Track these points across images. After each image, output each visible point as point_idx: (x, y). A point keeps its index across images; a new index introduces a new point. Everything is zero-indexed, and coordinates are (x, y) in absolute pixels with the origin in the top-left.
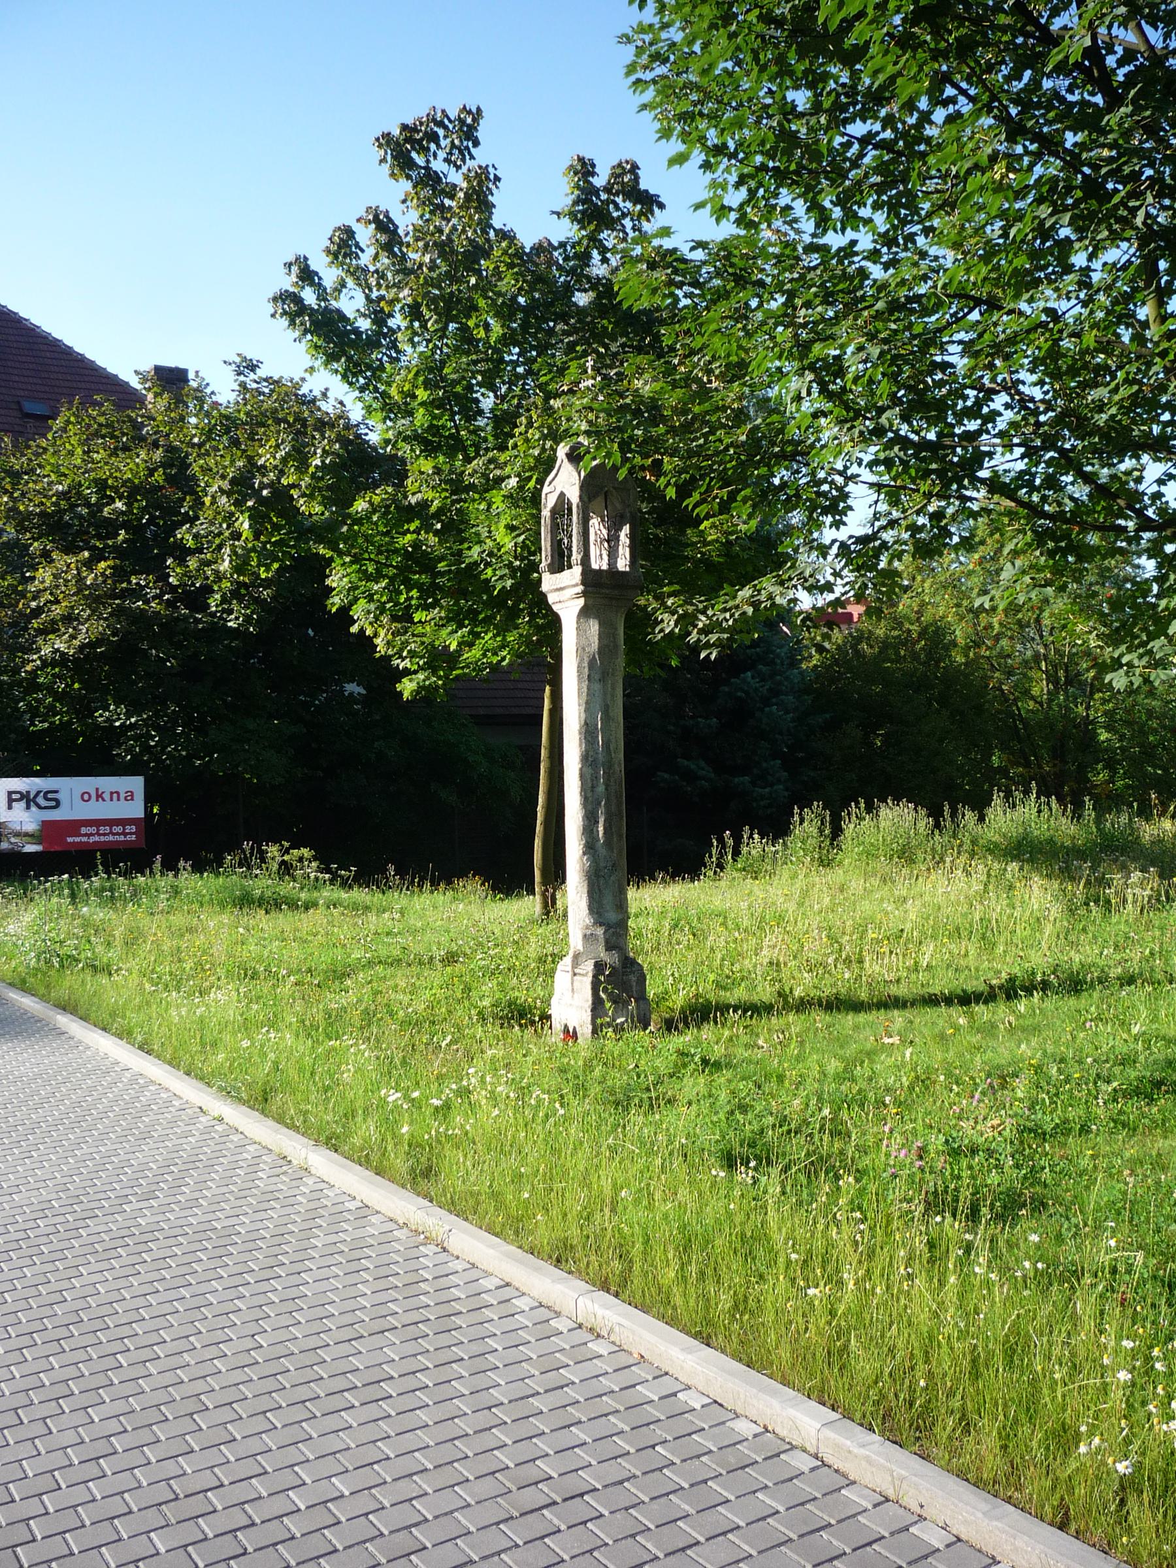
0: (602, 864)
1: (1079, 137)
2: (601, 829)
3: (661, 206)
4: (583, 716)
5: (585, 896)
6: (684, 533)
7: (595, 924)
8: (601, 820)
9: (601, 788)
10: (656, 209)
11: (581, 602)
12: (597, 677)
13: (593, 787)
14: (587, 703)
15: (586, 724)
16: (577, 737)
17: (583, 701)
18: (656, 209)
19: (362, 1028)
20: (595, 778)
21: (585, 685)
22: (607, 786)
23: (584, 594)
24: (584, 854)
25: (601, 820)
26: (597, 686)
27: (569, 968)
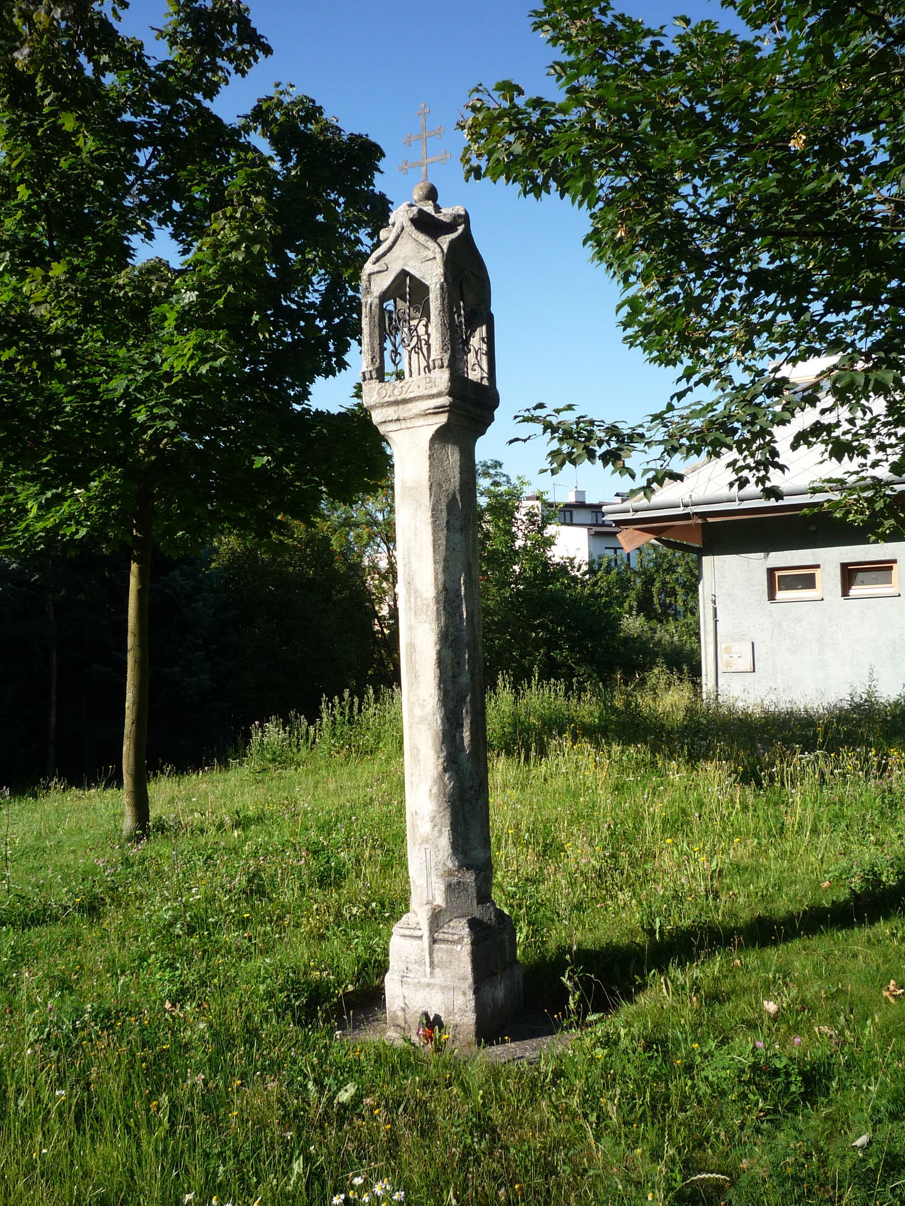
0: (468, 784)
1: (618, 235)
2: (466, 735)
3: (426, 1015)
4: (441, 577)
5: (446, 832)
6: (895, 391)
7: (460, 867)
8: (467, 722)
9: (465, 679)
10: (432, 1018)
11: (443, 419)
12: (458, 524)
13: (454, 677)
14: (446, 560)
15: (445, 588)
16: (433, 607)
17: (441, 558)
18: (432, 1018)
19: (59, 1155)
20: (457, 663)
21: (443, 534)
22: (473, 674)
23: (451, 410)
24: (445, 770)
25: (467, 722)
26: (457, 537)
27: (425, 931)
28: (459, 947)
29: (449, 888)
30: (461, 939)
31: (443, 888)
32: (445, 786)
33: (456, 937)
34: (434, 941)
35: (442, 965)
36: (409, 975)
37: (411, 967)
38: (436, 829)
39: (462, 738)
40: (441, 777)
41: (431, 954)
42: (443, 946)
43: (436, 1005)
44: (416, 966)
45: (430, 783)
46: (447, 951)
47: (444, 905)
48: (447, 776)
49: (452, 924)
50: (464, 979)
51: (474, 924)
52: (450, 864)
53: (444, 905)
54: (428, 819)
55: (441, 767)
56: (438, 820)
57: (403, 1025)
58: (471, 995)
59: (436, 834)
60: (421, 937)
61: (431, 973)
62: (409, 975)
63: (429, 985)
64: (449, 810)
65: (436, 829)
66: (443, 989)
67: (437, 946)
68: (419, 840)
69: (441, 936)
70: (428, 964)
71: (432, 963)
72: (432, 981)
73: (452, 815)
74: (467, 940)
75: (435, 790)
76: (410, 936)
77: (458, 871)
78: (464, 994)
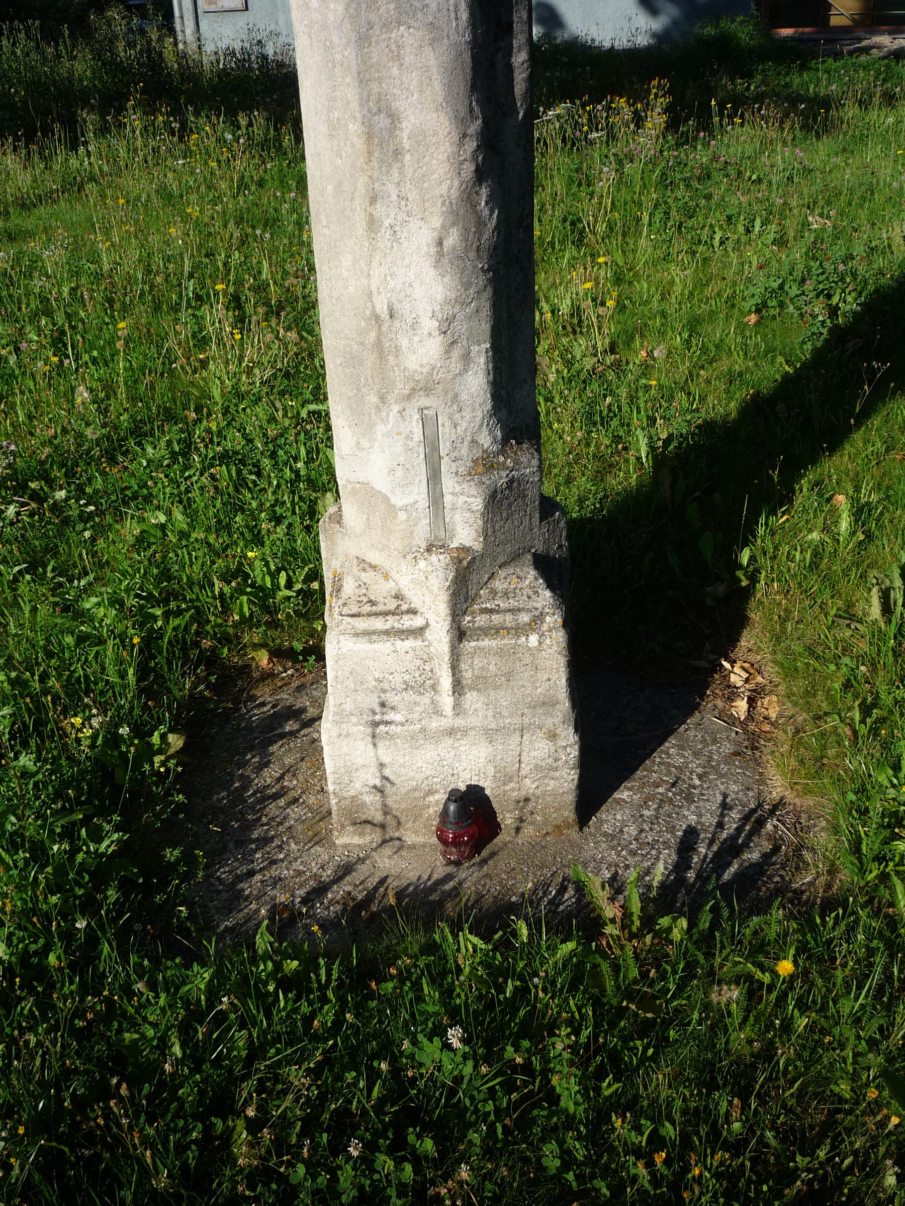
24: (480, 175)
28: (534, 639)
29: (496, 503)
30: (539, 618)
31: (478, 504)
32: (480, 223)
33: (525, 618)
34: (460, 635)
35: (482, 683)
36: (391, 716)
37: (392, 699)
38: (456, 353)
39: (510, 69)
40: (468, 197)
41: (455, 667)
42: (486, 643)
43: (471, 763)
44: (410, 696)
45: (437, 221)
46: (499, 652)
47: (478, 546)
48: (484, 192)
49: (499, 585)
50: (548, 703)
51: (544, 565)
52: (485, 440)
53: (478, 546)
54: (429, 325)
55: (469, 169)
56: (461, 327)
57: (378, 817)
58: (569, 738)
59: (455, 365)
60: (419, 632)
61: (457, 706)
62: (391, 716)
63: (451, 732)
64: (488, 294)
65: (456, 353)
66: (490, 735)
67: (469, 645)
68: (401, 388)
69: (482, 620)
70: (446, 682)
71: (458, 687)
72: (459, 722)
73: (496, 307)
74: (554, 620)
75: (453, 239)
76: (387, 633)
77: (502, 452)
78: (553, 736)
